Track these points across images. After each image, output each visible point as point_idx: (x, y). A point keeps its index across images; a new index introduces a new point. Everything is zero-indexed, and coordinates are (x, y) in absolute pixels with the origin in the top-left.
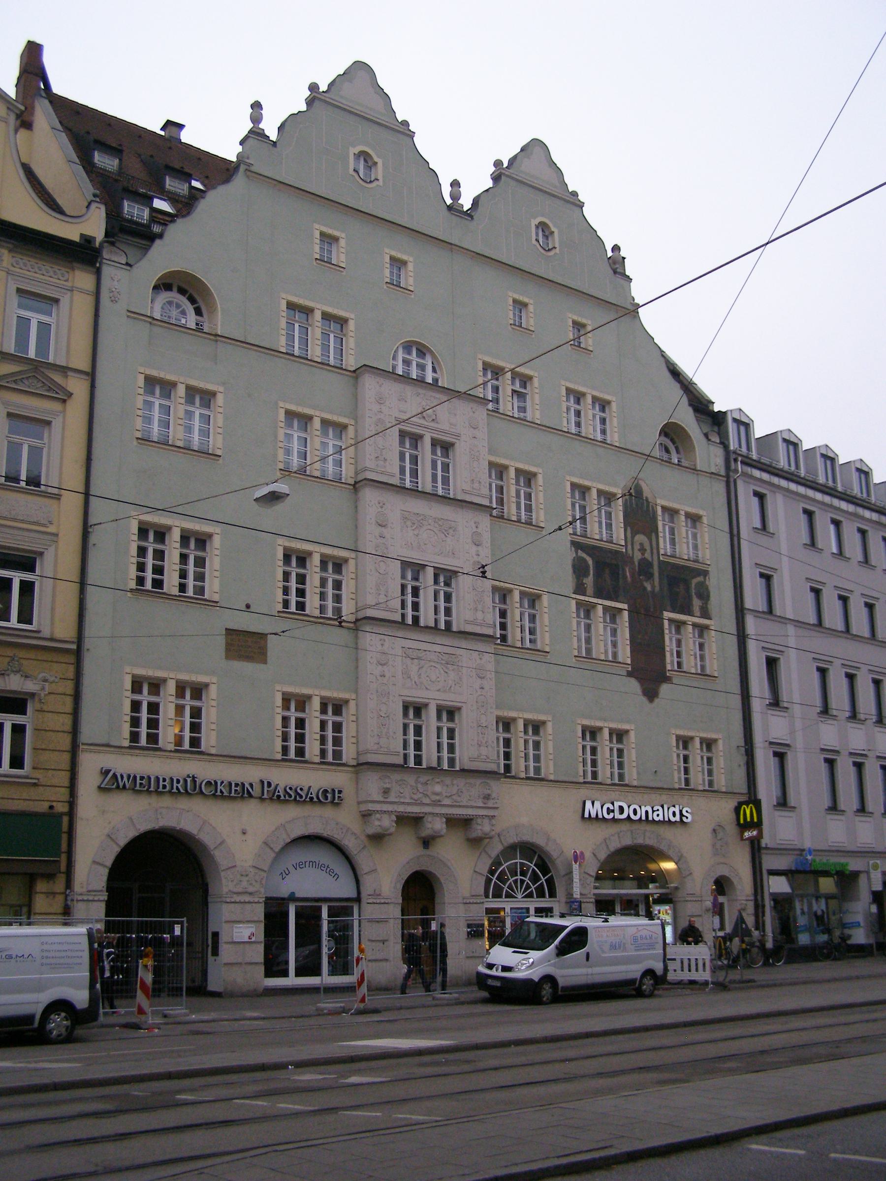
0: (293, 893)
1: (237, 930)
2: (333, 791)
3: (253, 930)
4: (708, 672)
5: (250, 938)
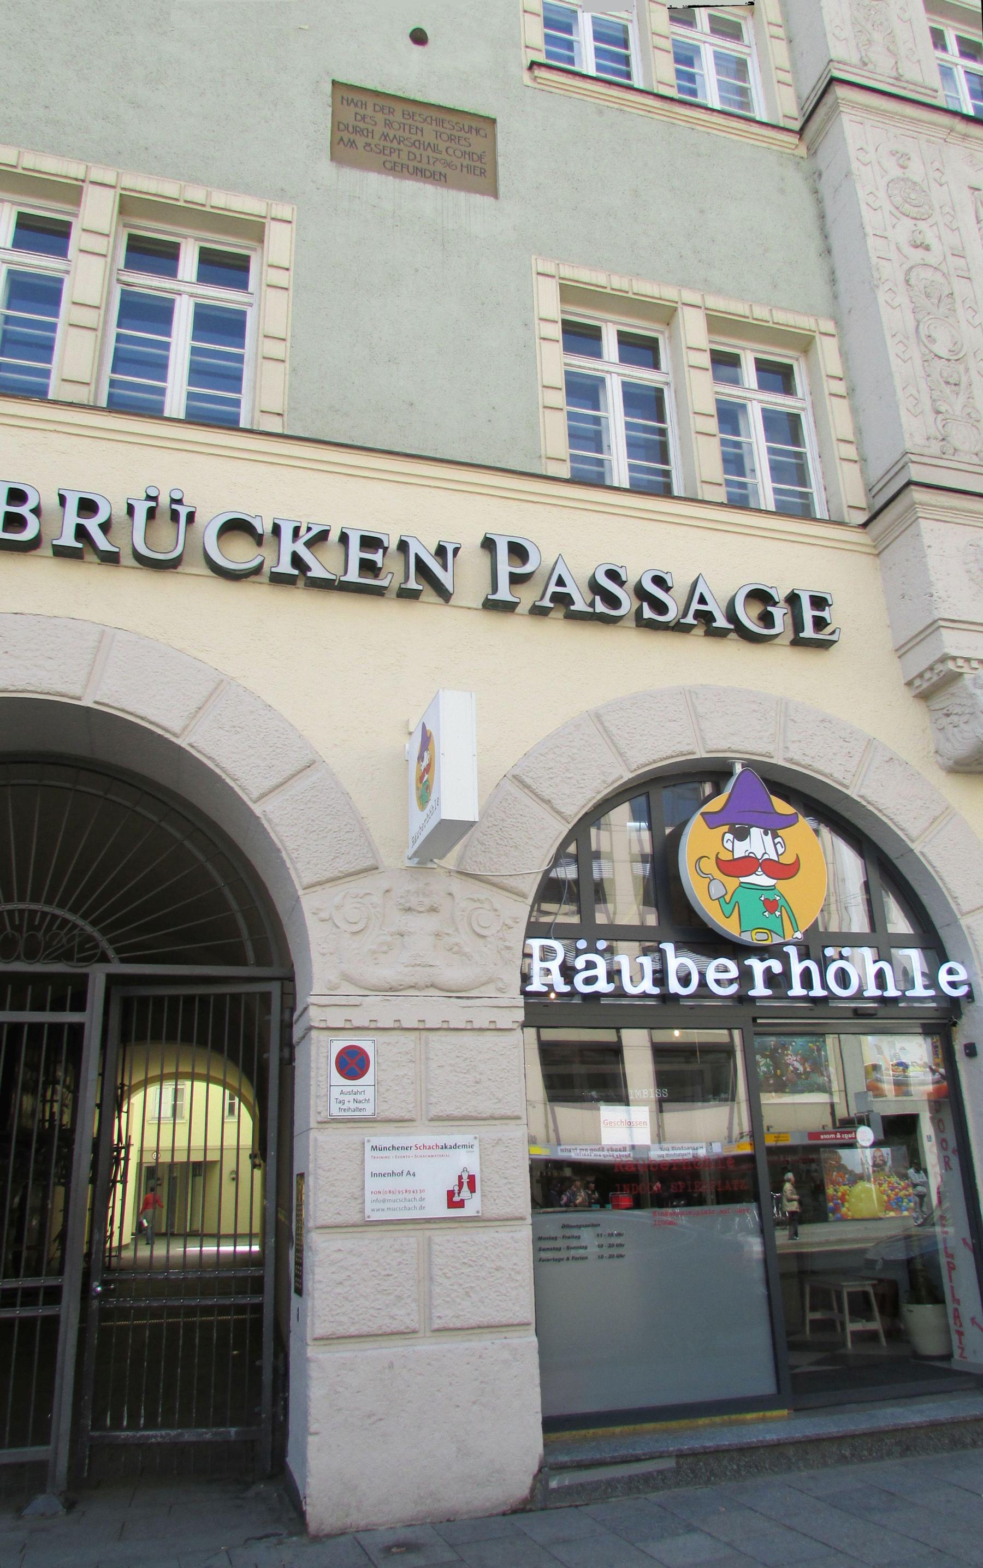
0: (644, 992)
1: (393, 1162)
2: (793, 599)
3: (469, 1161)
4: (614, 1031)
5: (453, 1202)
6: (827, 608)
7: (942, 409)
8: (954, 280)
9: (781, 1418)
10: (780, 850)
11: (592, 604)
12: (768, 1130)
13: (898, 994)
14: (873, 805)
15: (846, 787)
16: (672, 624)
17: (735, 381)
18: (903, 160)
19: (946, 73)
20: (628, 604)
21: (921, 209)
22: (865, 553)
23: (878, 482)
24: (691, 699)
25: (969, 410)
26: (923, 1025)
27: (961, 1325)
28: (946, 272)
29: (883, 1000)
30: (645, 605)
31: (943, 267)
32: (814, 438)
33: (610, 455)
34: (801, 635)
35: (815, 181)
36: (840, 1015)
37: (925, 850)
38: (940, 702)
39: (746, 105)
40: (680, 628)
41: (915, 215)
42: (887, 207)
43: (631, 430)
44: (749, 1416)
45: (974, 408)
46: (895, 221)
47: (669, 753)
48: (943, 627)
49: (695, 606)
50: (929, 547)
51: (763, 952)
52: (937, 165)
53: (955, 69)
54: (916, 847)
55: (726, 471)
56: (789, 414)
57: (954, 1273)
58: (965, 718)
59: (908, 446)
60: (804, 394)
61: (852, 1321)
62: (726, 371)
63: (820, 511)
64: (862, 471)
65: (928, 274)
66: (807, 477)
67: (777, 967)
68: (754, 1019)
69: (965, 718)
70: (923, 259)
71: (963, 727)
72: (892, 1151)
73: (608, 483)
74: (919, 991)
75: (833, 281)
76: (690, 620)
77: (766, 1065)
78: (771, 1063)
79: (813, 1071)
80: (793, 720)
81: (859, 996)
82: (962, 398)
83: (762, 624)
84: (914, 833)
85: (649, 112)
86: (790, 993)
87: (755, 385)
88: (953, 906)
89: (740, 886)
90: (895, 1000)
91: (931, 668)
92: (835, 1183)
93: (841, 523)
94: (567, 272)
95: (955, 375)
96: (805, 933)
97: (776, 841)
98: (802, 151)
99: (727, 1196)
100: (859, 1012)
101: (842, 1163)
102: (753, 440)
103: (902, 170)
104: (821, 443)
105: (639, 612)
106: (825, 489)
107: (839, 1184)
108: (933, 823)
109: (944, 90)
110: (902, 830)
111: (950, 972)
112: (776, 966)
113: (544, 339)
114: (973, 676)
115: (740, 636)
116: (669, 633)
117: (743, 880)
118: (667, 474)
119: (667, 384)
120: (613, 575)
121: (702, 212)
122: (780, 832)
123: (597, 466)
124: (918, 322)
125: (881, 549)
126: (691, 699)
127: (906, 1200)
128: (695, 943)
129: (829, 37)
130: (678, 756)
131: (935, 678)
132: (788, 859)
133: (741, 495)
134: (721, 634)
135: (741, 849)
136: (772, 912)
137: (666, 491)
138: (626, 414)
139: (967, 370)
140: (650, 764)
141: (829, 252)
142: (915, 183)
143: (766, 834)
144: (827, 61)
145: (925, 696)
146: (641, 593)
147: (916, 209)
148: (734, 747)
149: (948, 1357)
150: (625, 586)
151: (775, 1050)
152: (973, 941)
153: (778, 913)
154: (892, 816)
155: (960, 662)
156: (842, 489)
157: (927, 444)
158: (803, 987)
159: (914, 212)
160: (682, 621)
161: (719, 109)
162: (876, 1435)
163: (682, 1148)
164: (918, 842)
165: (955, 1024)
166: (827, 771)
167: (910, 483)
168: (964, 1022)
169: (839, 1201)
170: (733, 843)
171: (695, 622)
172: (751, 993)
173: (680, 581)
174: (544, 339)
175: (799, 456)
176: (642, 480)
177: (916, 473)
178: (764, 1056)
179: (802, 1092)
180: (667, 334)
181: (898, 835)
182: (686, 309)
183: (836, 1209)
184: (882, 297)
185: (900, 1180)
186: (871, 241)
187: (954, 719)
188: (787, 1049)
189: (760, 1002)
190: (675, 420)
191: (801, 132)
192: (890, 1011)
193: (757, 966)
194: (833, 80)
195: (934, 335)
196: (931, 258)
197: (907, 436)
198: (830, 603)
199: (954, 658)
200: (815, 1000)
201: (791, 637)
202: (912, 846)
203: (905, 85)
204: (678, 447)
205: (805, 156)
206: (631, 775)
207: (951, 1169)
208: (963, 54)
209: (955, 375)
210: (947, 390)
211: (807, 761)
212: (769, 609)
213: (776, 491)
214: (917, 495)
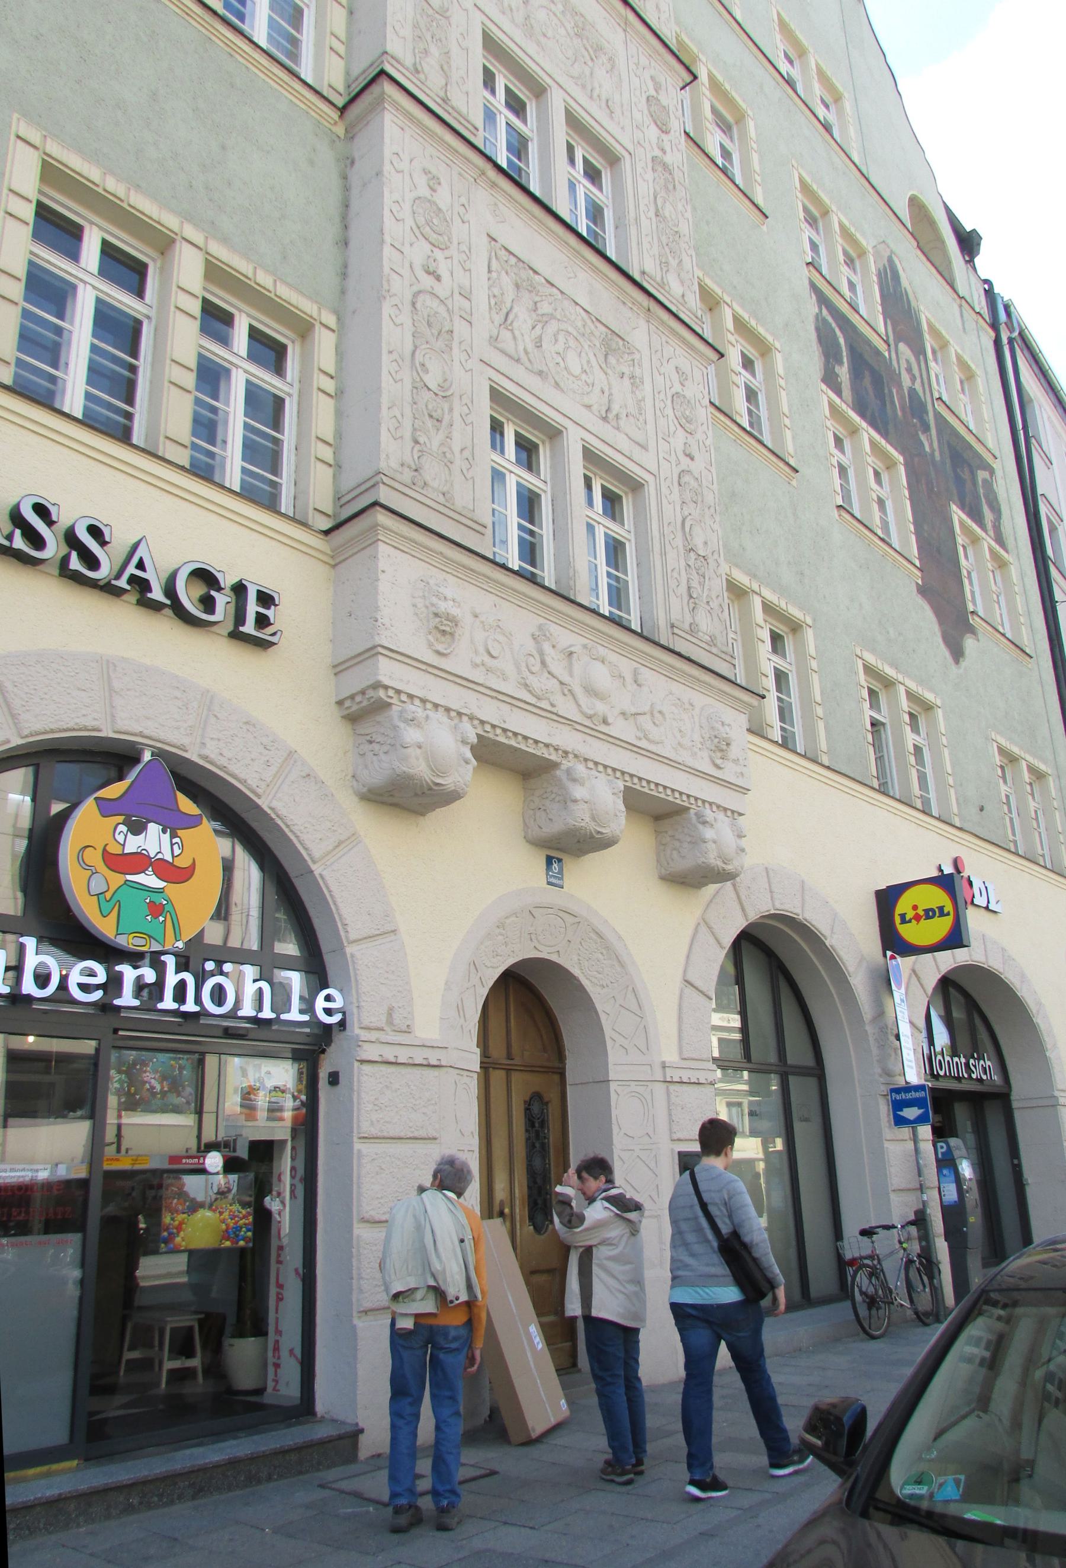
2: (240, 589)
6: (273, 607)
7: (421, 440)
8: (457, 320)
9: (70, 1470)
10: (177, 852)
11: (10, 537)
12: (127, 1152)
13: (273, 1016)
14: (281, 819)
15: (259, 796)
16: (102, 583)
17: (225, 341)
18: (434, 183)
19: (490, 116)
20: (53, 548)
21: (440, 238)
22: (322, 561)
23: (349, 492)
24: (108, 672)
25: (446, 449)
26: (294, 1050)
27: (279, 1358)
28: (451, 308)
29: (255, 1020)
30: (74, 555)
31: (449, 302)
32: (294, 428)
33: (66, 374)
34: (241, 629)
35: (346, 166)
36: (211, 1032)
37: (324, 873)
38: (366, 727)
39: (295, 57)
40: (109, 589)
41: (433, 241)
42: (409, 222)
43: (95, 354)
44: (31, 1472)
45: (450, 449)
46: (414, 239)
47: (71, 725)
48: (381, 654)
49: (131, 569)
50: (383, 571)
51: (134, 958)
52: (463, 200)
53: (498, 116)
54: (317, 869)
55: (194, 434)
56: (275, 396)
57: (280, 1304)
58: (386, 748)
59: (383, 465)
60: (293, 379)
61: (169, 1359)
62: (219, 326)
63: (286, 505)
64: (334, 476)
65: (434, 304)
66: (280, 468)
67: (149, 975)
68: (116, 1031)
69: (386, 748)
70: (432, 287)
71: (383, 757)
72: (239, 1178)
73: (57, 406)
74: (294, 1015)
75: (344, 275)
76: (123, 583)
77: (120, 1081)
78: (126, 1080)
79: (170, 1091)
80: (216, 716)
81: (232, 1015)
82: (441, 436)
83: (201, 607)
84: (317, 854)
85: (187, 14)
86: (160, 1006)
87: (244, 353)
88: (342, 933)
89: (125, 883)
90: (268, 1022)
91: (363, 692)
92: (174, 1211)
93: (304, 524)
94: (54, 149)
95: (439, 411)
96: (188, 944)
97: (175, 840)
98: (340, 130)
99: (54, 1225)
100: (230, 1032)
101: (185, 1189)
102: (231, 410)
103: (430, 192)
104: (300, 435)
105: (65, 561)
106: (295, 484)
107: (177, 1211)
108: (337, 846)
109: (485, 131)
110: (306, 849)
111: (328, 998)
112: (149, 975)
113: (11, 215)
114: (400, 708)
115: (176, 614)
116: (96, 592)
117: (129, 877)
118: (129, 416)
119: (148, 317)
120: (41, 510)
121: (223, 148)
122: (179, 832)
123: (49, 382)
124: (416, 347)
125: (338, 560)
126: (108, 672)
127: (244, 1229)
128: (64, 940)
129: (389, 29)
130: (80, 730)
131: (365, 703)
132: (183, 863)
133: (208, 464)
134: (155, 607)
135: (133, 844)
136: (156, 916)
137: (123, 435)
138: (94, 335)
139: (451, 410)
140: (46, 732)
141: (346, 244)
142: (440, 210)
143: (164, 831)
144: (380, 51)
145: (353, 719)
146: (71, 539)
147: (435, 236)
148: (146, 732)
149: (260, 1391)
150: (54, 527)
151: (134, 1064)
152: (355, 969)
153: (161, 919)
154: (299, 834)
155: (391, 693)
156: (311, 489)
157: (400, 470)
158: (175, 1000)
159: (433, 237)
160: (114, 582)
161: (265, 48)
162: (170, 1479)
163: (24, 1170)
164: (320, 863)
165: (323, 1051)
166: (242, 776)
167: (376, 504)
168: (332, 1050)
169: (175, 1231)
170: (126, 836)
171: (128, 587)
172: (117, 1002)
173: (121, 537)
174: (11, 215)
175: (277, 442)
176: (101, 414)
177: (384, 495)
178: (119, 1072)
179: (155, 1111)
180: (159, 264)
181: (301, 855)
182: (185, 245)
183: (171, 1237)
184: (387, 309)
185: (243, 1208)
186: (387, 250)
187: (376, 747)
188: (147, 1065)
189: (126, 1012)
190: (149, 359)
191: (343, 110)
192: (264, 1033)
193: (129, 973)
194: (382, 73)
195: (428, 365)
196: (442, 290)
197: (383, 456)
198: (277, 603)
199: (386, 688)
200: (186, 1015)
201: (231, 628)
202: (313, 867)
203: (451, 110)
204: (147, 390)
205: (342, 137)
206: (21, 742)
207: (296, 1198)
208: (508, 105)
209: (439, 411)
210: (429, 423)
211: (223, 762)
212: (213, 593)
213: (244, 471)
214: (381, 517)
